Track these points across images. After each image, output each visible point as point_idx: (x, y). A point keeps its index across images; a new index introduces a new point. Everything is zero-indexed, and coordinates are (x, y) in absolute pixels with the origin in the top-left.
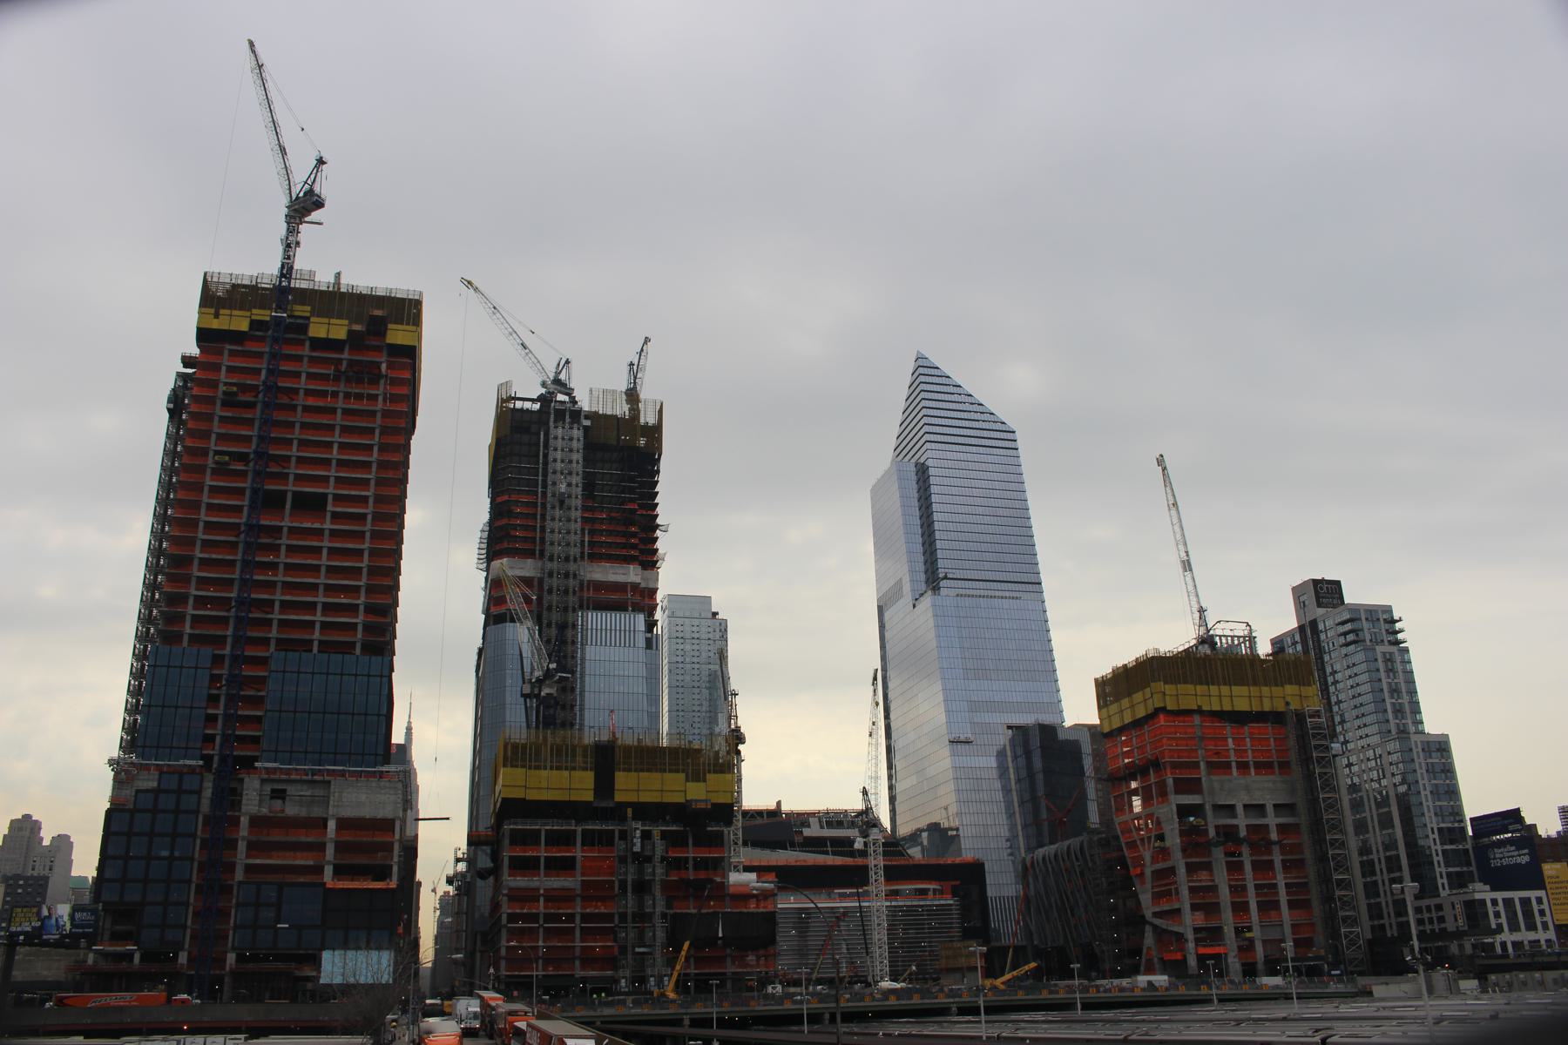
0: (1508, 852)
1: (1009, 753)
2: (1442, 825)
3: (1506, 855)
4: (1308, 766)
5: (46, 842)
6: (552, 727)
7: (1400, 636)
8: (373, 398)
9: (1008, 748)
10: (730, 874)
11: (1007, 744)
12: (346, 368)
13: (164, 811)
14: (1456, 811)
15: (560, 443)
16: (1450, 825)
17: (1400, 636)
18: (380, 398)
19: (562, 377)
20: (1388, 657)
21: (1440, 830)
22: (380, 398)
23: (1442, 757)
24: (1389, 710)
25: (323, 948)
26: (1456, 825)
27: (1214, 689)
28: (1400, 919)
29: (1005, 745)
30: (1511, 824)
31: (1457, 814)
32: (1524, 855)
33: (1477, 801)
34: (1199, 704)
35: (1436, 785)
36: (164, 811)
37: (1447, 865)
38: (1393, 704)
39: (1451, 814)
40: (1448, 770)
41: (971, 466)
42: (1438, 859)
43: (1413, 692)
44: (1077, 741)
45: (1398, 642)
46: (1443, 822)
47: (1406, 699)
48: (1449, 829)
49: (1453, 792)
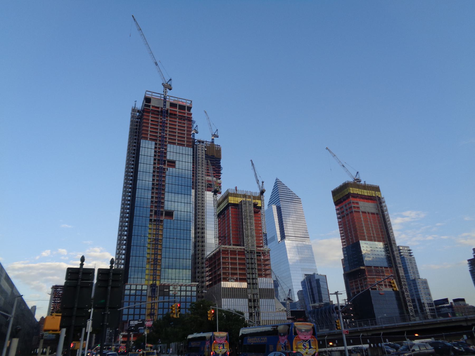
0: (446, 309)
1: (306, 282)
2: (428, 302)
3: (445, 310)
4: (379, 201)
7: (412, 254)
9: (306, 280)
10: (229, 197)
11: (305, 279)
14: (426, 282)
15: (200, 190)
16: (430, 302)
17: (412, 254)
18: (186, 124)
20: (410, 259)
21: (428, 303)
22: (186, 124)
26: (431, 302)
27: (360, 190)
28: (416, 309)
30: (445, 302)
32: (450, 310)
33: (436, 296)
34: (357, 192)
37: (428, 307)
39: (430, 299)
42: (426, 305)
43: (416, 268)
45: (411, 256)
46: (428, 301)
49: (429, 295)
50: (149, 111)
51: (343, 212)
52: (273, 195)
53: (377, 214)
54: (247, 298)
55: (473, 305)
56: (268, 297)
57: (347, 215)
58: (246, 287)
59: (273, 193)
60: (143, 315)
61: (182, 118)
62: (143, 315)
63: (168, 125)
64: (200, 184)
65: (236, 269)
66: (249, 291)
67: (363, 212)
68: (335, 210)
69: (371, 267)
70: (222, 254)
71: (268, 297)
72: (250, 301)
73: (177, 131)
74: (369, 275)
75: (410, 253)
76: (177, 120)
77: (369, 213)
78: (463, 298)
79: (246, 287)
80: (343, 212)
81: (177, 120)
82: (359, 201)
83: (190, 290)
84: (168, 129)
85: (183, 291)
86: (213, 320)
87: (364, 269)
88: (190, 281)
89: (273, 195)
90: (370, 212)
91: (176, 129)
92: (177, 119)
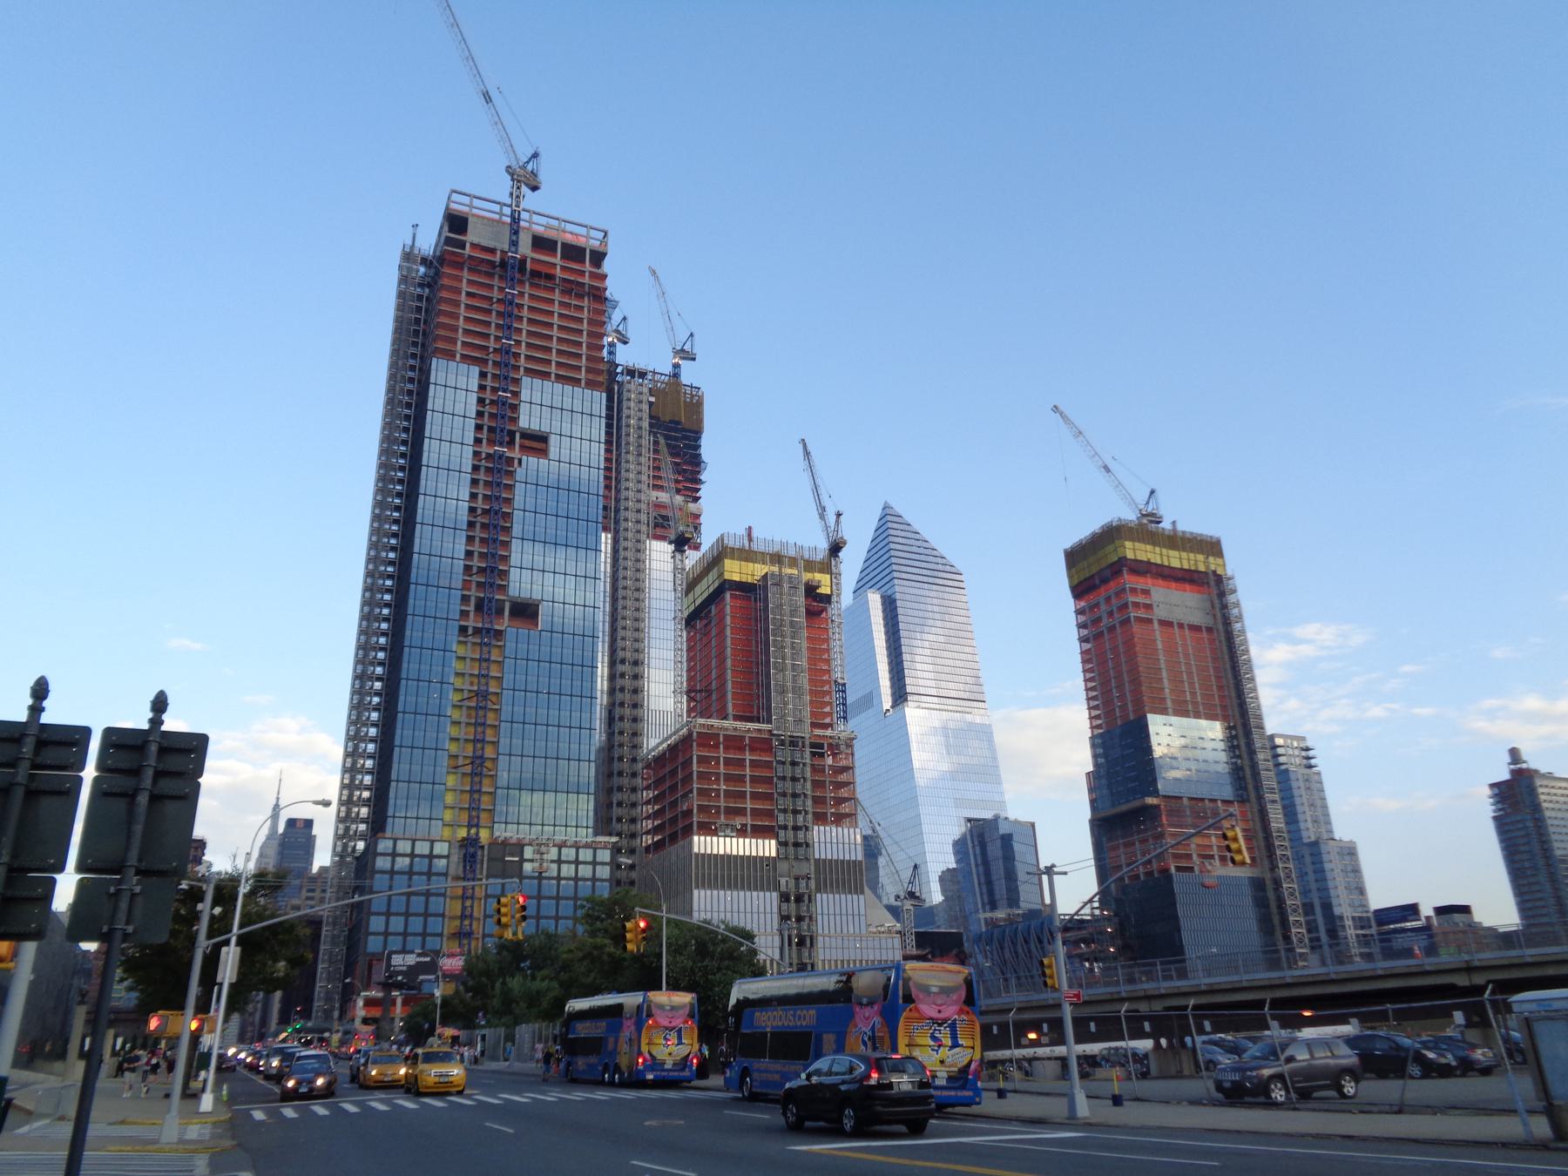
5: (315, 869)
6: (735, 954)
8: (581, 308)
12: (969, 1090)
13: (547, 918)
18: (586, 309)
19: (620, 328)
21: (1353, 918)
22: (586, 309)
23: (1352, 860)
24: (1309, 819)
29: (754, 944)
30: (1410, 915)
31: (1364, 906)
33: (1381, 896)
35: (1349, 882)
36: (547, 918)
38: (1312, 816)
40: (1356, 871)
41: (928, 572)
44: (1351, 842)
47: (1319, 813)
48: (1359, 917)
49: (1361, 891)
51: (1097, 621)
53: (1209, 630)
54: (775, 890)
57: (1112, 629)
58: (774, 854)
59: (879, 532)
65: (742, 795)
66: (783, 867)
67: (1163, 623)
68: (1074, 615)
69: (1181, 798)
72: (785, 898)
73: (555, 332)
74: (1171, 825)
75: (1309, 758)
76: (557, 296)
77: (1181, 626)
79: (774, 854)
80: (1097, 621)
82: (1153, 585)
84: (524, 326)
87: (1157, 807)
90: (1186, 622)
92: (557, 291)
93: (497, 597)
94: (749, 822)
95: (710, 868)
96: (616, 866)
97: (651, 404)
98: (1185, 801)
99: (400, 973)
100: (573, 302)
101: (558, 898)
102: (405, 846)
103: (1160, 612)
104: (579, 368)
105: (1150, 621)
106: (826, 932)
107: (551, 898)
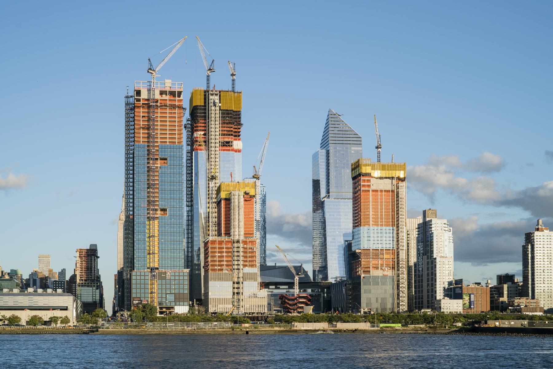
25: (175, 306)
50: (139, 105)
52: (325, 136)
53: (393, 191)
54: (231, 281)
55: (71, 275)
56: (213, 279)
59: (325, 133)
60: (147, 280)
61: (173, 107)
62: (147, 280)
63: (159, 128)
64: (213, 133)
65: (223, 256)
67: (373, 191)
69: (369, 250)
70: (211, 244)
71: (221, 280)
73: (168, 124)
76: (168, 111)
77: (381, 191)
78: (496, 276)
81: (168, 111)
83: (137, 276)
84: (159, 124)
85: (138, 275)
86: (378, 355)
88: (183, 267)
89: (325, 136)
91: (166, 125)
92: (168, 109)
93: (155, 208)
94: (248, 255)
95: (213, 276)
96: (382, 225)
97: (220, 107)
98: (371, 251)
99: (135, 304)
100: (173, 112)
101: (145, 293)
102: (138, 274)
103: (373, 188)
104: (175, 134)
105: (369, 191)
106: (246, 291)
107: (145, 290)
